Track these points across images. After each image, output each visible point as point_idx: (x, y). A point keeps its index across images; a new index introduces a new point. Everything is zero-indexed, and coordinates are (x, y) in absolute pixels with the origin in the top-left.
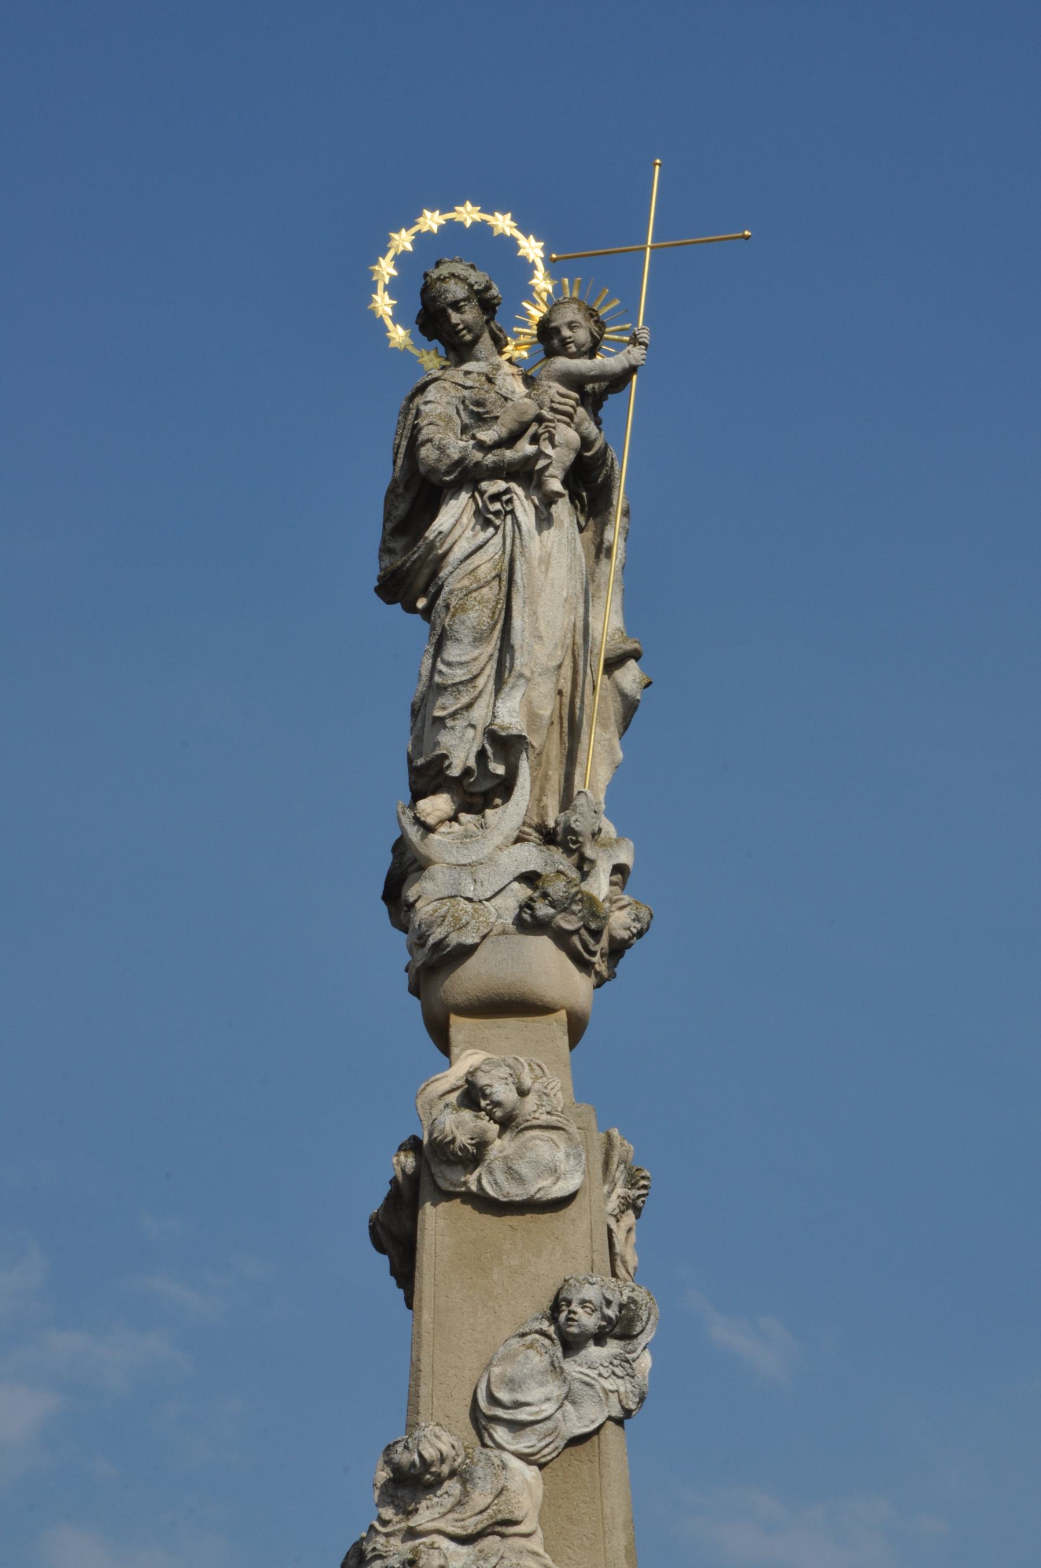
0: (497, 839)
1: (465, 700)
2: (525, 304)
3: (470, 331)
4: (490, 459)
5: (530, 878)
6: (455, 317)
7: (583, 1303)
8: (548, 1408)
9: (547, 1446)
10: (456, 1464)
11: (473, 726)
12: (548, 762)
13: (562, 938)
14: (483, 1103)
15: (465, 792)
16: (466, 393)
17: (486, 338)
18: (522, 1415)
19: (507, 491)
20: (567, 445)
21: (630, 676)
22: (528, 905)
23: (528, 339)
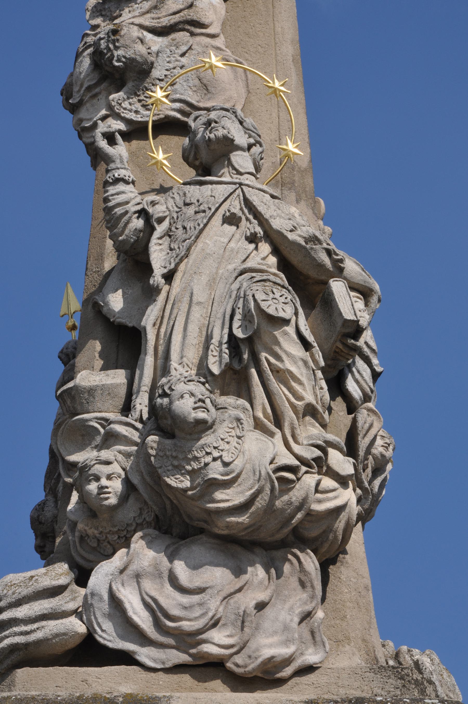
2: (350, 482)
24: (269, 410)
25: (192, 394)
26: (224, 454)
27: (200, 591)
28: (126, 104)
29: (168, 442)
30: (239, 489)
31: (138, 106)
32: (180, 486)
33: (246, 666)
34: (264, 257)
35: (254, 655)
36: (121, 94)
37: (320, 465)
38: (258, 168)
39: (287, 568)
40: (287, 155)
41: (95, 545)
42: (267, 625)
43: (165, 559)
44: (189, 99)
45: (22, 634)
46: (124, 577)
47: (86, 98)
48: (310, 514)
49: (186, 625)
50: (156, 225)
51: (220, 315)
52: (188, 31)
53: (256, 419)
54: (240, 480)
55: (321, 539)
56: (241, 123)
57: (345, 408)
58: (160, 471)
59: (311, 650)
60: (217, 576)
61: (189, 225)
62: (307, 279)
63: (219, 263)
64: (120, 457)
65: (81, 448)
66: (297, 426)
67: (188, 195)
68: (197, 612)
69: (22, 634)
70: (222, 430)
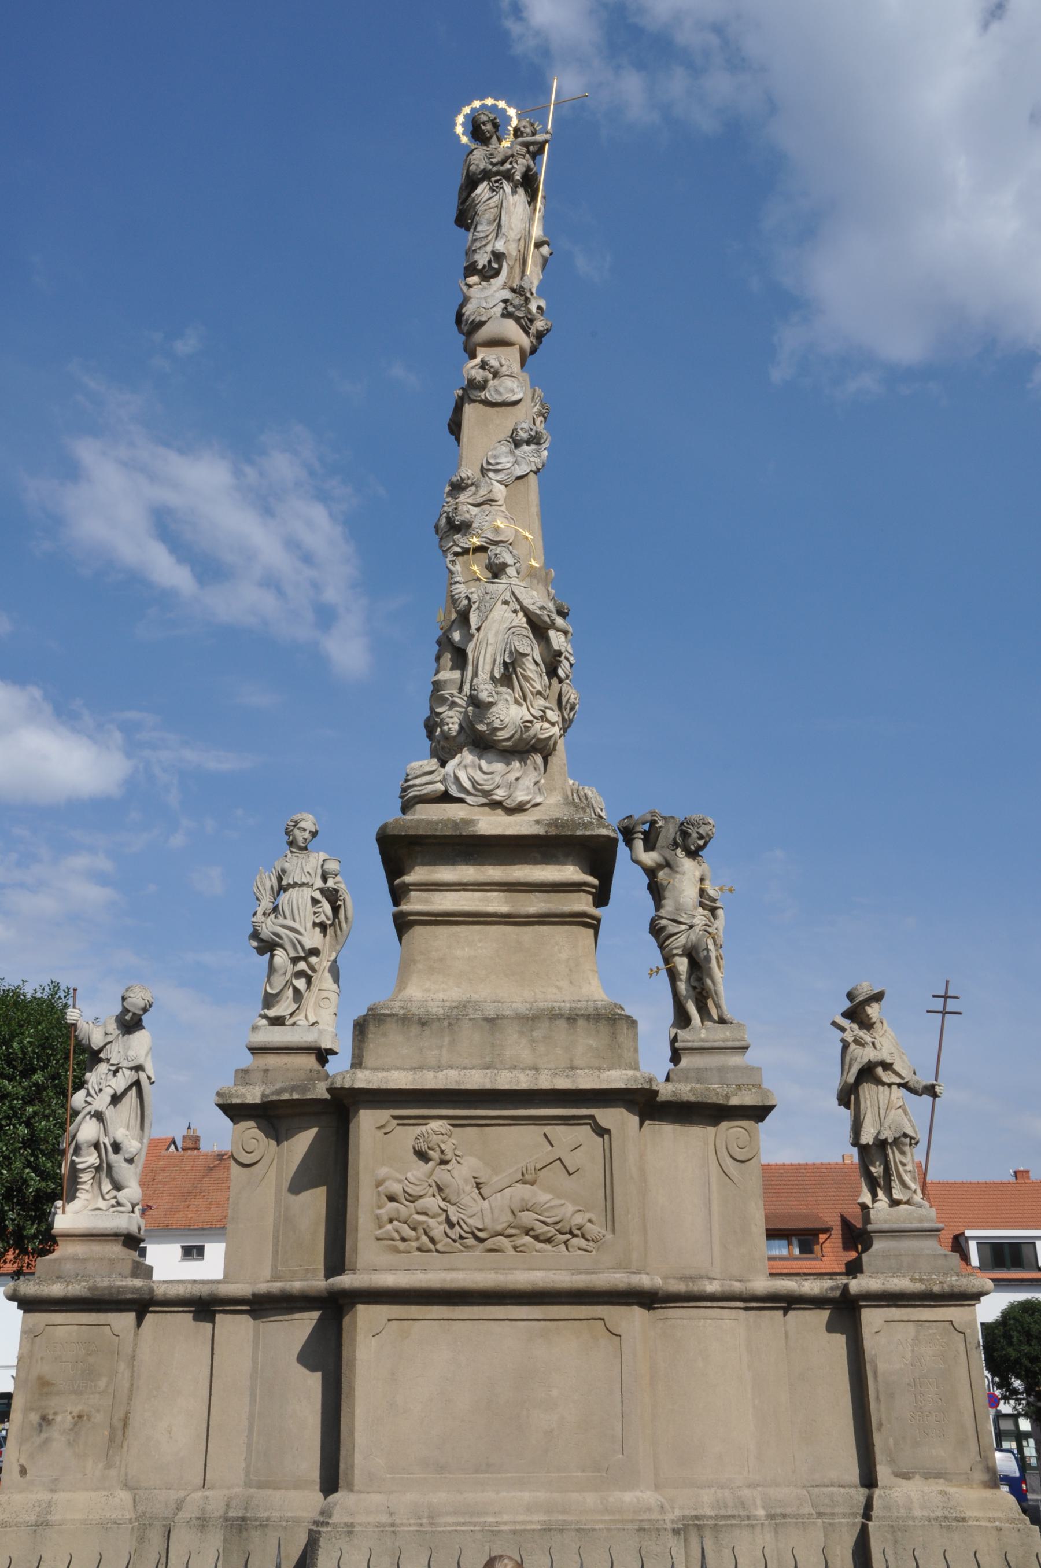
1: (484, 243)
4: (494, 169)
5: (505, 301)
6: (483, 127)
7: (522, 429)
8: (509, 465)
13: (518, 320)
18: (499, 467)
20: (523, 164)
21: (545, 250)
22: (506, 308)
34: (521, 619)
37: (543, 718)
39: (529, 761)
40: (532, 566)
42: (520, 786)
48: (539, 740)
49: (486, 788)
55: (544, 749)
60: (499, 767)
62: (539, 628)
65: (442, 705)
68: (491, 782)
70: (501, 705)
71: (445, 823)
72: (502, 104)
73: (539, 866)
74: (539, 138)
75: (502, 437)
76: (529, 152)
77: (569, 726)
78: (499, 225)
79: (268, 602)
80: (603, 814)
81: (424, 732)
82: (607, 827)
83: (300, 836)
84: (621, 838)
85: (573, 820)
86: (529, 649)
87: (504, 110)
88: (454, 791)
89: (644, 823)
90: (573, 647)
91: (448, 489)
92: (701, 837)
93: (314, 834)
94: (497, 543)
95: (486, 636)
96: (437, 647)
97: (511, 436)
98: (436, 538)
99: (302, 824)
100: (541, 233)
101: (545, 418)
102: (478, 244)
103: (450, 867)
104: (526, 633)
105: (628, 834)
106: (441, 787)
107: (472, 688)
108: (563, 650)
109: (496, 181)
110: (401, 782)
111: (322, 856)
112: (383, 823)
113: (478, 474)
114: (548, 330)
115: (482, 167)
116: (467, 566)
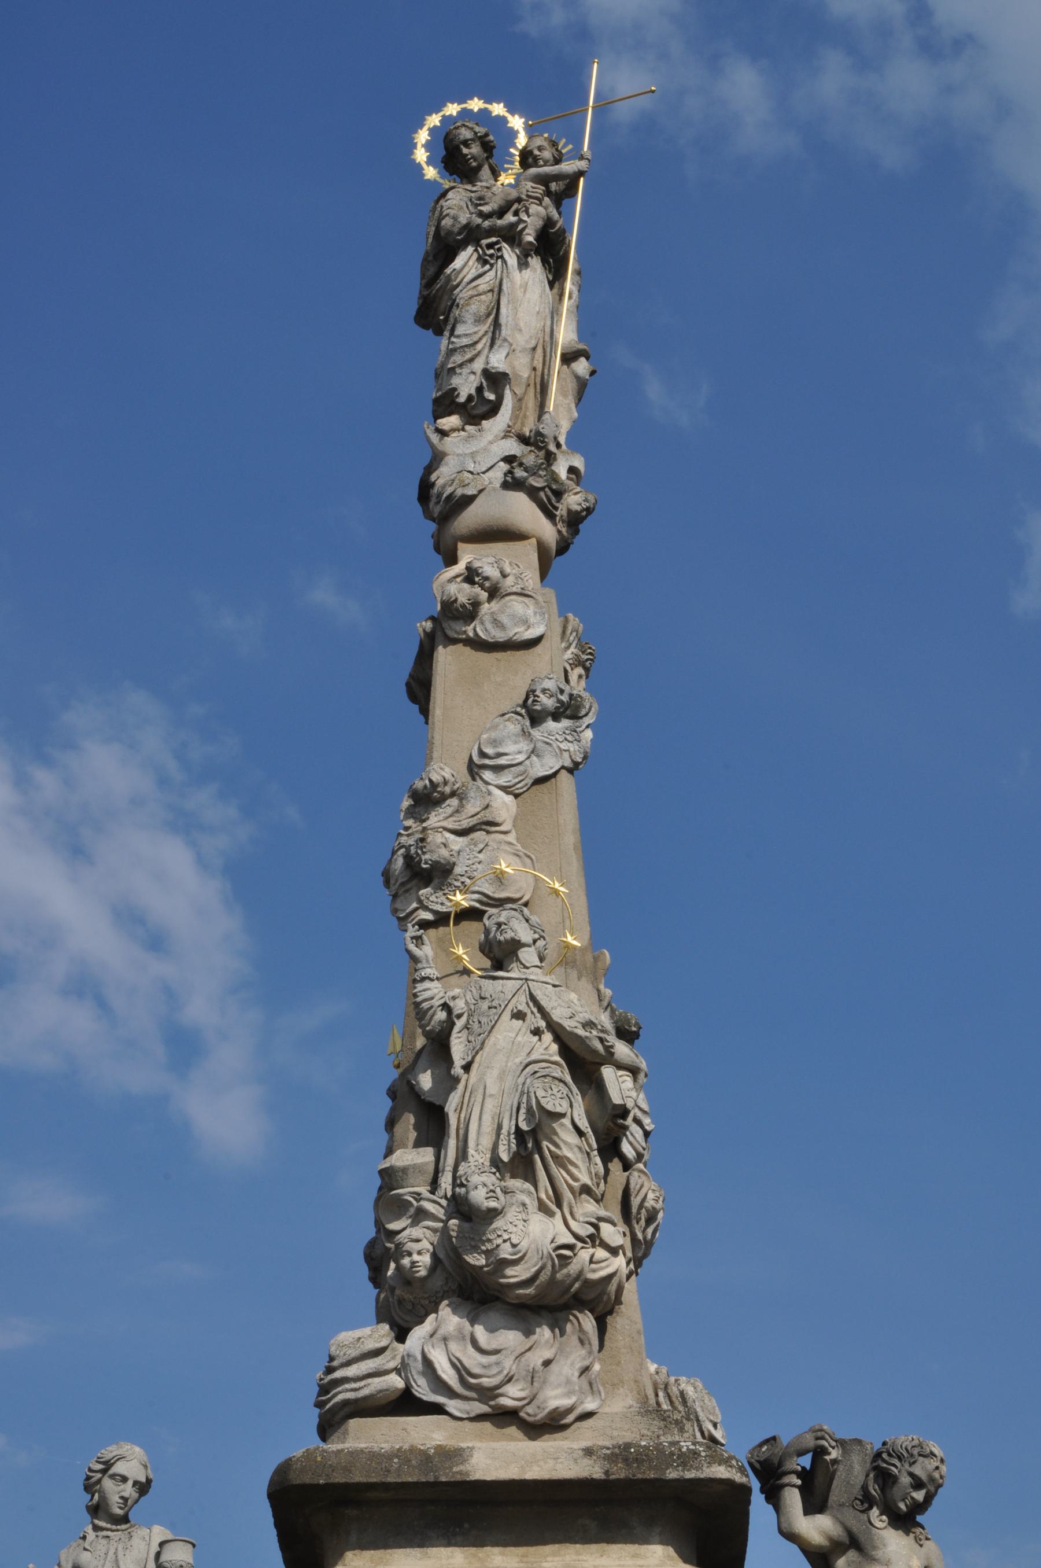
0: (490, 438)
1: (468, 356)
3: (475, 160)
4: (487, 224)
5: (509, 459)
6: (465, 151)
7: (544, 691)
8: (521, 758)
9: (520, 782)
10: (455, 787)
11: (474, 373)
12: (526, 408)
13: (533, 493)
14: (477, 579)
15: (469, 415)
16: (473, 195)
17: (486, 167)
18: (502, 761)
19: (497, 243)
20: (538, 215)
21: (582, 367)
22: (510, 472)
23: (514, 171)
24: (551, 1192)
25: (485, 1185)
26: (513, 1236)
27: (496, 1352)
28: (433, 898)
29: (466, 1225)
30: (526, 1266)
31: (443, 899)
32: (477, 1263)
33: (535, 1415)
34: (548, 1047)
35: (542, 1406)
36: (429, 890)
37: (595, 1239)
38: (542, 959)
39: (569, 1327)
40: (568, 946)
41: (410, 1308)
42: (552, 1378)
43: (467, 1324)
44: (486, 891)
45: (352, 1390)
46: (434, 1339)
47: (401, 892)
48: (587, 1283)
49: (486, 1382)
50: (456, 1020)
51: (508, 1107)
52: (484, 830)
53: (539, 1200)
54: (526, 1258)
55: (598, 1301)
56: (527, 921)
57: (621, 1168)
58: (460, 1250)
59: (589, 1399)
60: (510, 1338)
61: (484, 1020)
62: (582, 1064)
63: (508, 1057)
64: (428, 1233)
65: (398, 1217)
66: (574, 1205)
67: (484, 989)
68: (494, 1370)
69: (352, 1390)
70: (512, 1213)
71: (404, 1456)
72: (498, 109)
73: (594, 1547)
74: (568, 167)
75: (507, 705)
76: (548, 193)
77: (646, 1255)
78: (497, 325)
79: (80, 1021)
80: (718, 1434)
81: (364, 1270)
82: (726, 1462)
83: (114, 1492)
84: (755, 1485)
85: (659, 1447)
86: (565, 1104)
87: (503, 120)
88: (423, 1391)
89: (801, 1454)
90: (649, 1099)
91: (407, 803)
92: (918, 1484)
93: (143, 1488)
94: (500, 903)
95: (481, 1079)
96: (389, 1103)
97: (524, 705)
98: (386, 895)
99: (119, 1468)
100: (573, 336)
101: (587, 670)
102: (457, 358)
103: (416, 1552)
104: (557, 1073)
105: (770, 1474)
106: (396, 1382)
107: (456, 1182)
108: (630, 1104)
109: (490, 246)
110: (320, 1374)
111: (159, 1533)
112: (281, 1459)
113: (464, 775)
114: (589, 511)
115: (463, 220)
116: (444, 947)
